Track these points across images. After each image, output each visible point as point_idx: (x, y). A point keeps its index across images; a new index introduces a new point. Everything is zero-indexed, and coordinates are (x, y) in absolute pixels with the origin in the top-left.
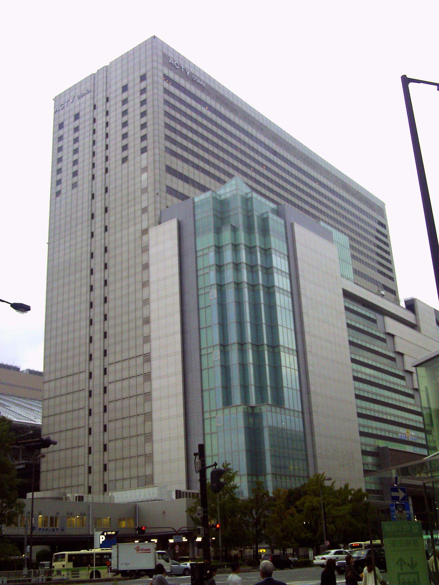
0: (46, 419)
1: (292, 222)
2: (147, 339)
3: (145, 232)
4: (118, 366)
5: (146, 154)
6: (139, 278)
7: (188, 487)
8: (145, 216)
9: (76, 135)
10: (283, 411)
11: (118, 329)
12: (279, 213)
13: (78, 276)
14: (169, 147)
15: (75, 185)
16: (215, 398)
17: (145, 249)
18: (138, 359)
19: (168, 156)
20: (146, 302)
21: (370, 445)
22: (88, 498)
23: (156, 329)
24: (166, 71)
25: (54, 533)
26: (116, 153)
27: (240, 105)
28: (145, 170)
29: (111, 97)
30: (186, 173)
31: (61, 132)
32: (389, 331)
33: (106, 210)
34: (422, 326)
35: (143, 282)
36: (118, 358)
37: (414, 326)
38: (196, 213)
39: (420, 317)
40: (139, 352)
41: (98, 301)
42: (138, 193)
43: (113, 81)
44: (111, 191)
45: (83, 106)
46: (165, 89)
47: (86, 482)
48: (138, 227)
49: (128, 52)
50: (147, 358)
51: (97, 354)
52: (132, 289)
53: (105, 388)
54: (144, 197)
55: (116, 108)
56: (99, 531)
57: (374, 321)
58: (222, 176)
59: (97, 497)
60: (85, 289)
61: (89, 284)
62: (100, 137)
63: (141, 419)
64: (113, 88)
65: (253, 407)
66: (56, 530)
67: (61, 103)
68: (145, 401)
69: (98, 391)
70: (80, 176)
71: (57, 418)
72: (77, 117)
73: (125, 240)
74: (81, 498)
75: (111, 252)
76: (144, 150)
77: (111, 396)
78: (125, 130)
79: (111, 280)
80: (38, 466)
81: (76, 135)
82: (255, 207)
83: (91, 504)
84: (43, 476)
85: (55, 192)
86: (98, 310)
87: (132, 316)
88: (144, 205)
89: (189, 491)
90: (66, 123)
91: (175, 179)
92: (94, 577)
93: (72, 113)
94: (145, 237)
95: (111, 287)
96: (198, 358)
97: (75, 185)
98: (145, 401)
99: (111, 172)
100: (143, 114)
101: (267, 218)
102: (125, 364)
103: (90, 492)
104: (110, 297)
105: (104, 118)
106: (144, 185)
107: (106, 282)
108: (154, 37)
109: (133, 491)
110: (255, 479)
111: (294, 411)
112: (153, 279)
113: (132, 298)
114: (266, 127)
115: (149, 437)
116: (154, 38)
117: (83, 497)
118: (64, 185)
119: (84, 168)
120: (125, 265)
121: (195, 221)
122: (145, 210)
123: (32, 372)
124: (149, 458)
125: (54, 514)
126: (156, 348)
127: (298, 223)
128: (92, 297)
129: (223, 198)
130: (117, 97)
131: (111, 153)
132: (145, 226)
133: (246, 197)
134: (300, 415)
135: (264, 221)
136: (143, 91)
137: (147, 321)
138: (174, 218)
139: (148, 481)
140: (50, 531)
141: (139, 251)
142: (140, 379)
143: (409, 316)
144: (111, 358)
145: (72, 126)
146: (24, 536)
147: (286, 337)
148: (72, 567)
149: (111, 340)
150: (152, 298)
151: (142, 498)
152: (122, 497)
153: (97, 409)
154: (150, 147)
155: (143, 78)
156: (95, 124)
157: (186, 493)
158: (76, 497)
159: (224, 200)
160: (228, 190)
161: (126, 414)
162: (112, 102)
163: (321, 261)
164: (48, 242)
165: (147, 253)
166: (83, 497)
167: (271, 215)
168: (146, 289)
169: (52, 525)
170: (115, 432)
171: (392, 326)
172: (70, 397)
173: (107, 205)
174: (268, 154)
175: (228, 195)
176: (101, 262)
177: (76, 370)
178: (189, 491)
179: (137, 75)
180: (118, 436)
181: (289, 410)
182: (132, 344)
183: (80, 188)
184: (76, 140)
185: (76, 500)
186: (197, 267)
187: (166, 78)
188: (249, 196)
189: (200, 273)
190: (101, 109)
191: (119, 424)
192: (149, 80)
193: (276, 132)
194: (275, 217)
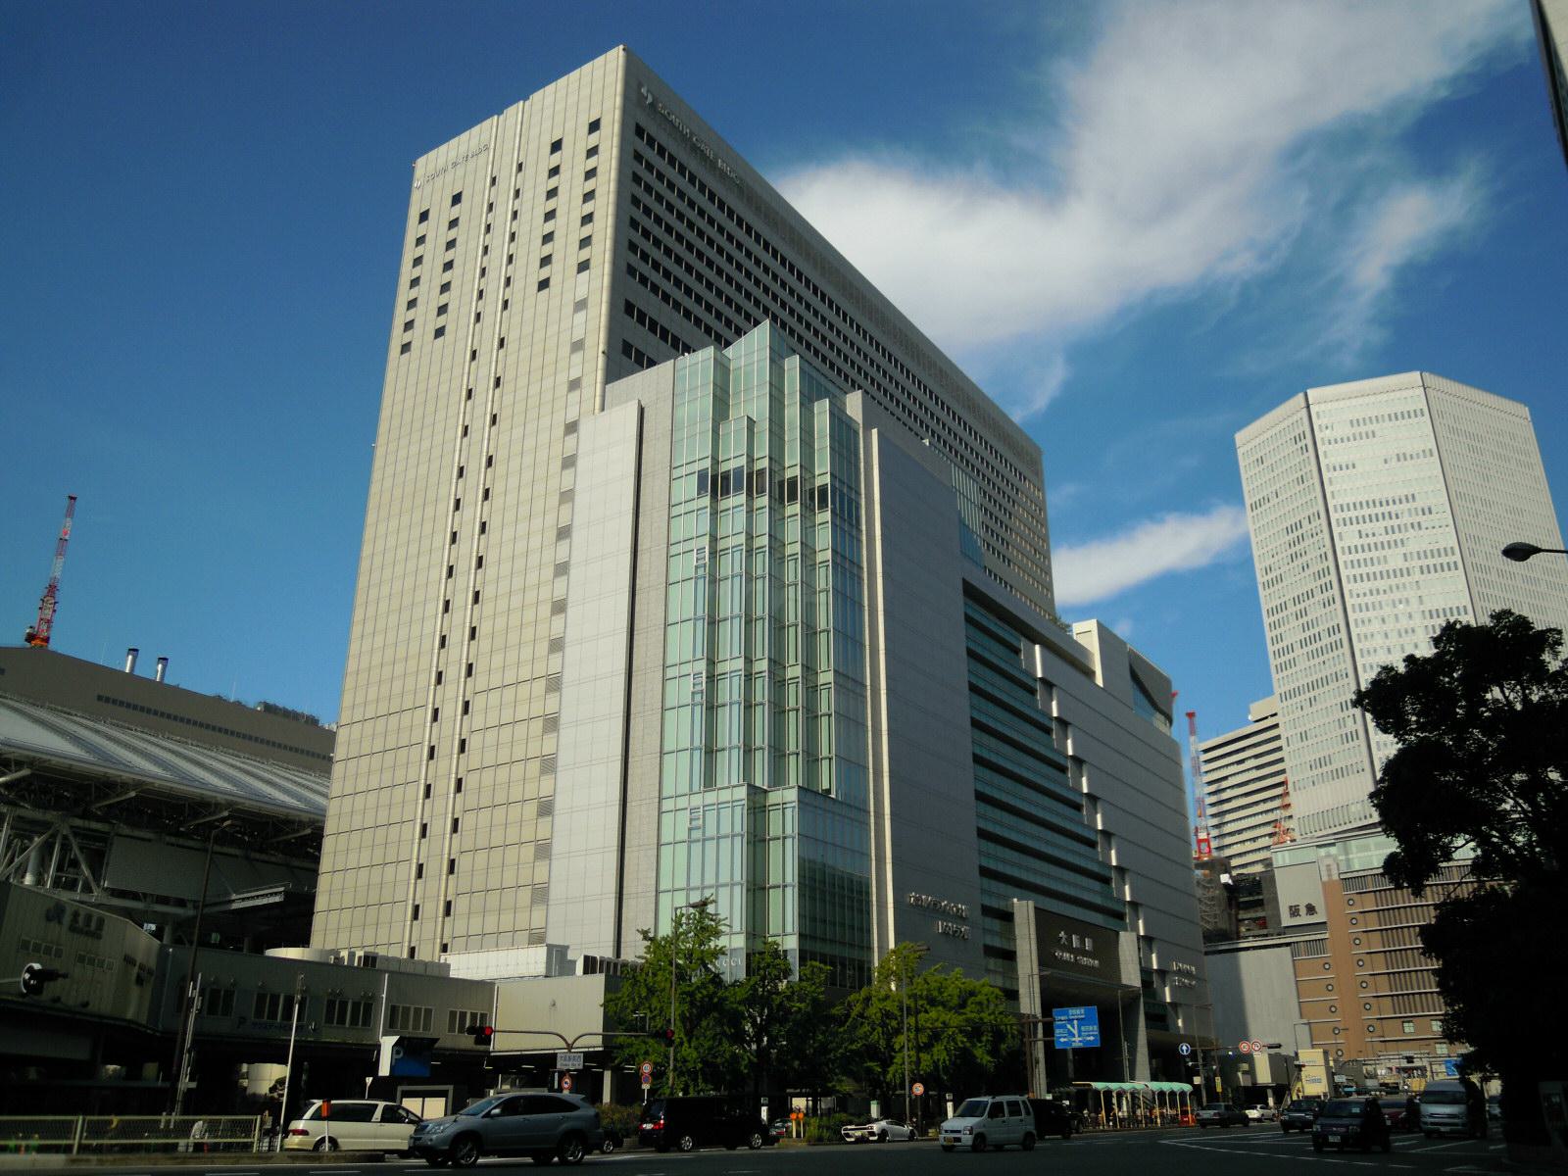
3: (572, 428)
5: (584, 312)
6: (551, 519)
11: (501, 622)
16: (682, 770)
18: (536, 684)
35: (558, 529)
51: (454, 673)
84: (328, 844)
87: (531, 596)
109: (502, 954)
113: (531, 596)
122: (574, 385)
131: (518, 271)
144: (480, 680)
165: (567, 537)
180: (484, 802)
189: (667, 805)
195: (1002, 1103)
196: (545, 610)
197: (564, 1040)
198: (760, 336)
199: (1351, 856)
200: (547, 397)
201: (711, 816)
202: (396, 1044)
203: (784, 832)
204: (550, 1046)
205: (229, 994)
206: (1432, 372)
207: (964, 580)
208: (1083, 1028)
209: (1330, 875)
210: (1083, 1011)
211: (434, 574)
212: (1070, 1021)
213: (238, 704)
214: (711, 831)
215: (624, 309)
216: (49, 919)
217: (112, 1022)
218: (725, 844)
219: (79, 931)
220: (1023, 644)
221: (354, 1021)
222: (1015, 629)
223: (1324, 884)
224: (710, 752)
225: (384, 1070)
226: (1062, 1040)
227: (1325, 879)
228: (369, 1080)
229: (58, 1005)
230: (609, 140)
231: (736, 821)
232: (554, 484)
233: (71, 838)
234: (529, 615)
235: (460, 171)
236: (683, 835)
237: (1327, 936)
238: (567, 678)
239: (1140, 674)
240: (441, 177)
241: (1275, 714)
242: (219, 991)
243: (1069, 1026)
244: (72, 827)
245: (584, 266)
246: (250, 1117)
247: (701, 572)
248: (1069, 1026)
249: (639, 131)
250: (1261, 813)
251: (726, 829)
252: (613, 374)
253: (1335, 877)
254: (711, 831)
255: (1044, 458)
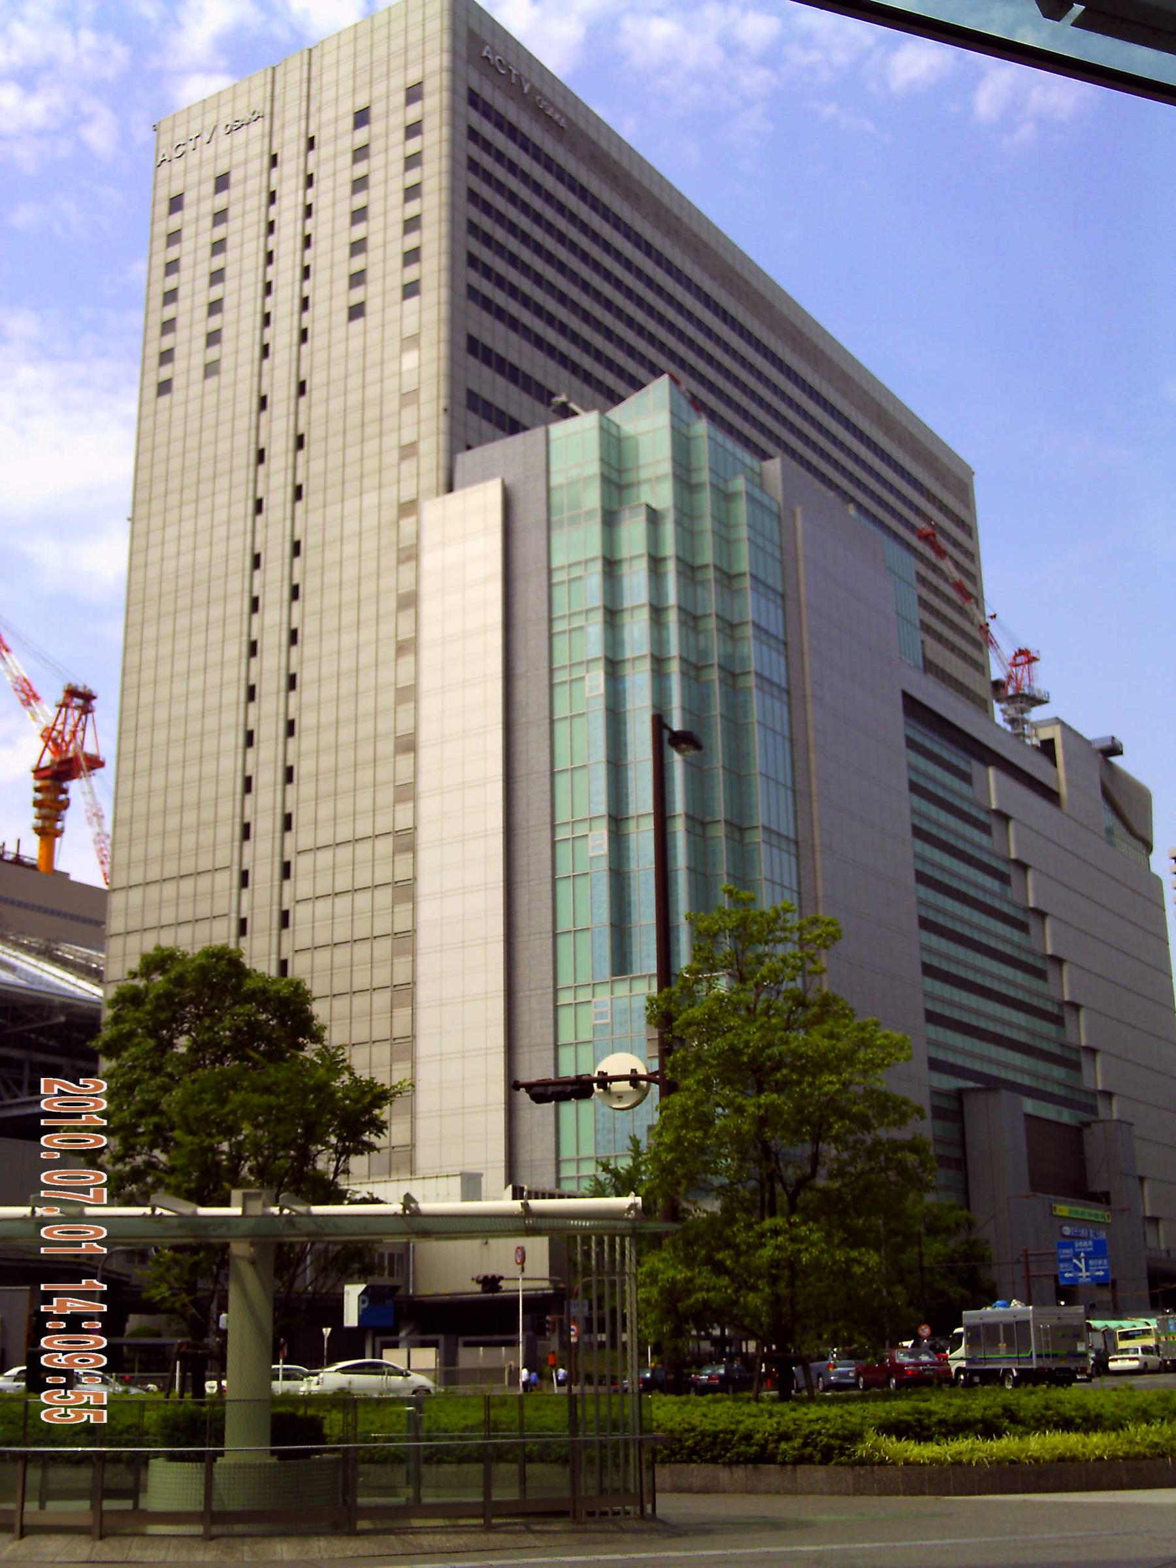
6: (387, 628)
11: (327, 761)
26: (332, 296)
35: (397, 642)
60: (236, 649)
87: (366, 728)
99: (317, 340)
113: (366, 728)
196: (387, 747)
198: (659, 391)
200: (371, 464)
202: (364, 1293)
212: (1077, 1256)
215: (470, 349)
220: (975, 768)
225: (351, 1319)
228: (327, 1331)
230: (434, 108)
232: (388, 582)
234: (366, 753)
239: (1116, 796)
245: (411, 290)
249: (474, 99)
252: (460, 441)
255: (975, 478)
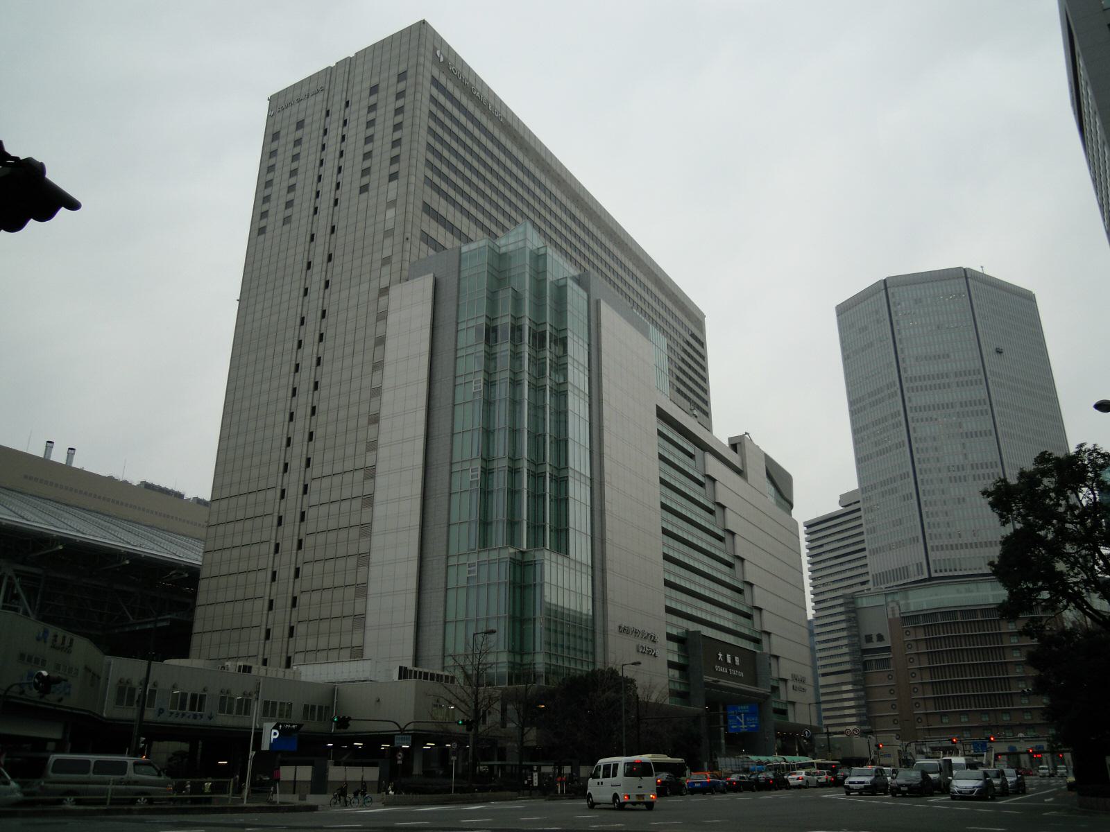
0: (209, 556)
1: (598, 298)
2: (372, 446)
3: (384, 291)
4: (326, 482)
7: (416, 663)
8: (386, 269)
9: (297, 150)
10: (566, 560)
12: (581, 281)
13: (279, 348)
14: (431, 178)
15: (287, 220)
16: (464, 536)
17: (382, 316)
19: (428, 189)
20: (377, 392)
21: (677, 626)
22: (258, 670)
23: (387, 432)
24: (436, 73)
25: (195, 722)
26: (352, 179)
27: (532, 144)
28: (392, 204)
29: (354, 100)
30: (450, 218)
31: (274, 146)
32: (710, 472)
33: (330, 258)
34: (750, 472)
36: (327, 471)
37: (740, 472)
38: (463, 267)
39: (748, 461)
40: (359, 464)
41: (302, 412)
42: (380, 237)
43: (358, 79)
44: (340, 232)
45: (309, 111)
46: (431, 96)
47: (261, 653)
48: (375, 284)
49: (383, 40)
50: (370, 473)
51: (296, 464)
52: (357, 372)
53: (303, 514)
54: (388, 242)
55: (358, 116)
56: (271, 722)
57: (691, 456)
58: (507, 224)
59: (276, 671)
60: (288, 368)
61: (294, 362)
62: (331, 155)
63: (352, 562)
64: (357, 88)
65: (523, 553)
66: (199, 717)
67: (280, 104)
68: (361, 535)
69: (291, 517)
70: (296, 208)
71: (226, 554)
72: (300, 125)
73: (353, 302)
74: (247, 669)
75: (331, 319)
76: (393, 177)
77: (310, 526)
78: (368, 148)
79: (326, 358)
80: (190, 625)
81: (297, 150)
82: (549, 268)
83: (262, 680)
84: (203, 585)
85: (257, 228)
86: (301, 425)
87: (354, 410)
88: (387, 253)
89: (416, 669)
90: (283, 133)
91: (434, 224)
92: (245, 801)
93: (294, 120)
94: (383, 300)
95: (326, 367)
96: (448, 477)
97: (287, 220)
98: (361, 535)
99: (343, 204)
100: (399, 111)
101: (566, 286)
102: (337, 480)
103: (265, 662)
104: (324, 382)
105: (340, 129)
106: (389, 225)
107: (316, 384)
108: (424, 22)
109: (332, 666)
110: (518, 659)
111: (581, 564)
112: (389, 357)
113: (354, 410)
114: (564, 181)
115: (362, 589)
116: (424, 23)
117: (250, 668)
118: (271, 219)
119: (304, 198)
120: (350, 338)
121: (459, 279)
122: (386, 261)
123: (199, 501)
124: (360, 620)
125: (199, 692)
126: (385, 459)
127: (607, 302)
128: (296, 380)
129: (503, 250)
130: (361, 100)
131: (345, 179)
132: (384, 283)
133: (536, 252)
134: (590, 570)
135: (561, 289)
136: (400, 95)
137: (375, 419)
138: (429, 272)
139: (357, 653)
140: (189, 717)
141: (372, 319)
142: (357, 504)
143: (734, 458)
144: (316, 470)
145: (291, 138)
146: (133, 721)
147: (578, 459)
148: (378, 768)
149: (318, 443)
150: (384, 413)
151: (345, 677)
152: (316, 673)
153: (288, 545)
154: (402, 174)
155: (402, 76)
156: (324, 153)
157: (411, 671)
158: (240, 666)
159: (505, 254)
160: (512, 240)
161: (330, 554)
162: (353, 107)
163: (631, 360)
164: (239, 298)
166: (250, 668)
167: (570, 283)
168: (377, 375)
169: (192, 708)
170: (312, 578)
171: (714, 467)
172: (248, 524)
173: (332, 251)
174: (565, 217)
175: (511, 248)
176: (315, 331)
177: (262, 485)
178: (416, 669)
179: (394, 71)
181: (575, 561)
182: (350, 451)
183: (294, 224)
184: (296, 157)
185: (239, 671)
186: (456, 345)
187: (435, 82)
188: (542, 251)
189: (453, 561)
190: (336, 116)
191: (318, 567)
192: (410, 81)
193: (578, 191)
194: (576, 287)
195: (94, 773)
197: (398, 725)
199: (909, 601)
201: (484, 570)
203: (489, 579)
204: (376, 730)
205: (202, 697)
206: (980, 273)
207: (657, 405)
208: (748, 719)
209: (894, 614)
210: (747, 707)
211: (282, 393)
212: (739, 714)
213: (125, 482)
214: (484, 580)
216: (38, 639)
217: (69, 710)
218: (494, 590)
219: (58, 648)
221: (239, 712)
222: (684, 436)
223: (890, 621)
224: (485, 523)
226: (733, 727)
227: (890, 616)
229: (23, 696)
231: (501, 574)
233: (15, 578)
235: (303, 104)
236: (463, 582)
237: (891, 656)
238: (379, 469)
240: (289, 108)
241: (858, 502)
242: (186, 694)
243: (738, 717)
244: (15, 570)
246: (226, 780)
247: (477, 397)
248: (738, 717)
250: (470, 509)
251: (494, 579)
253: (897, 616)
254: (484, 580)
